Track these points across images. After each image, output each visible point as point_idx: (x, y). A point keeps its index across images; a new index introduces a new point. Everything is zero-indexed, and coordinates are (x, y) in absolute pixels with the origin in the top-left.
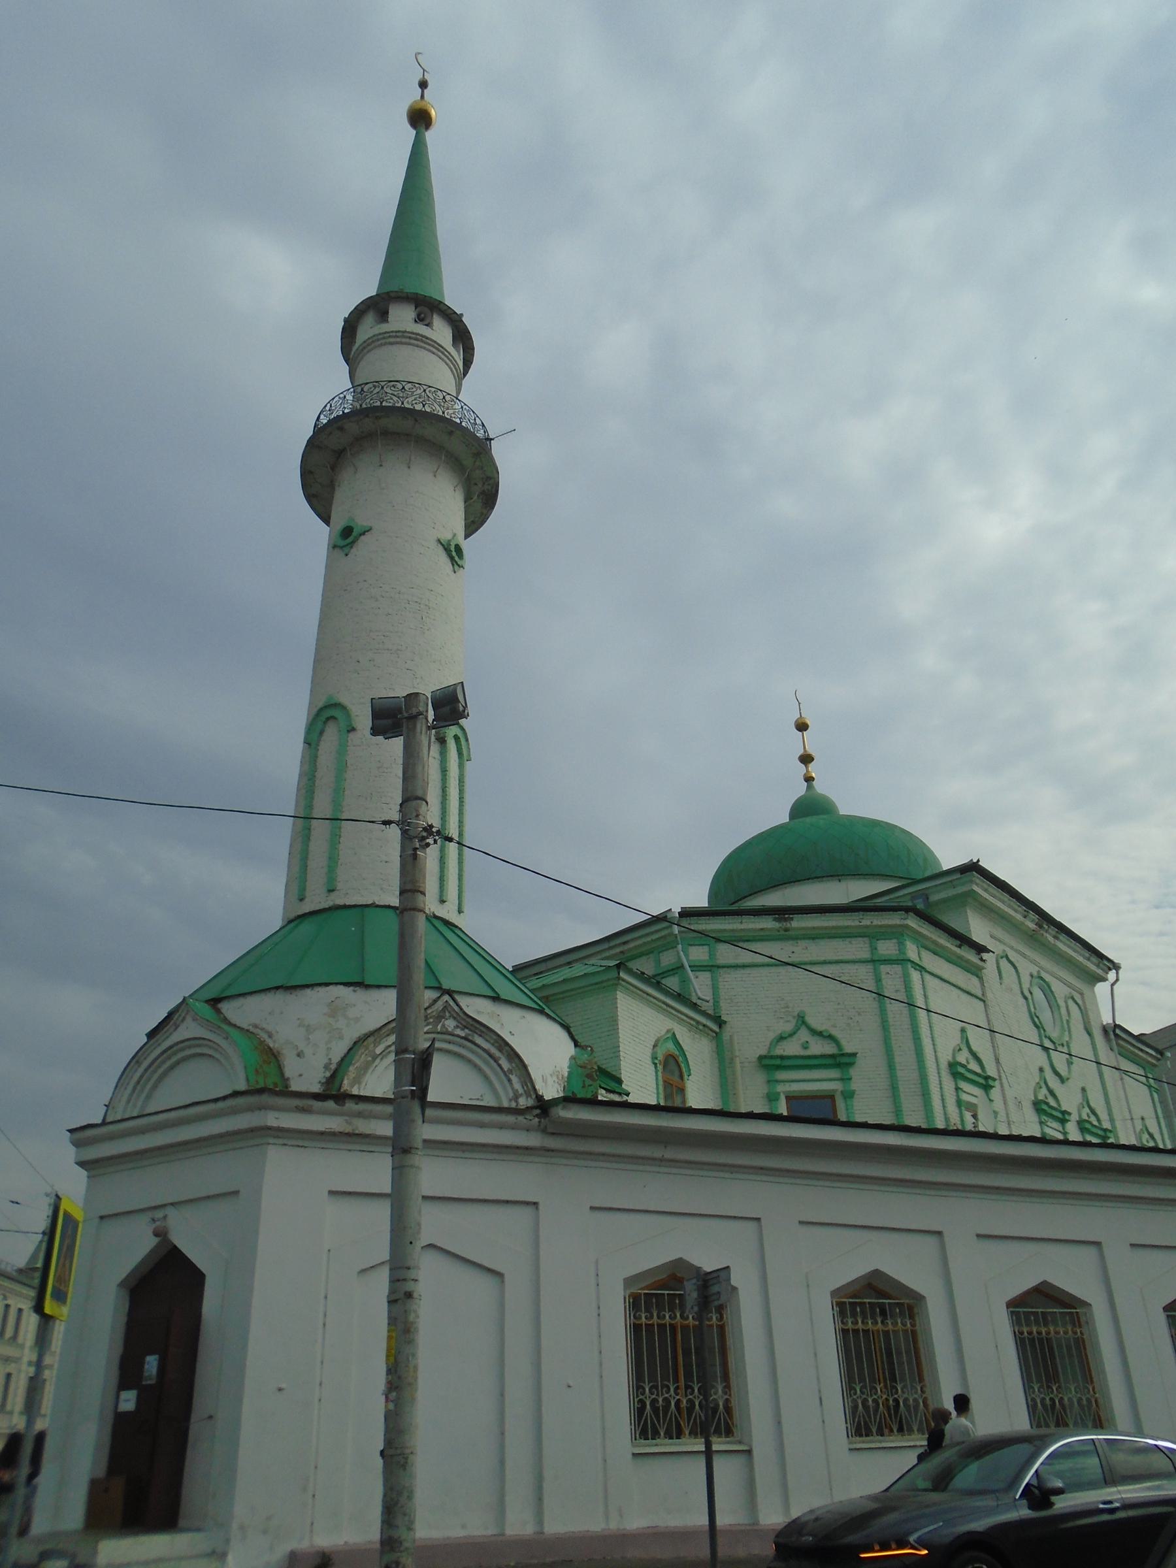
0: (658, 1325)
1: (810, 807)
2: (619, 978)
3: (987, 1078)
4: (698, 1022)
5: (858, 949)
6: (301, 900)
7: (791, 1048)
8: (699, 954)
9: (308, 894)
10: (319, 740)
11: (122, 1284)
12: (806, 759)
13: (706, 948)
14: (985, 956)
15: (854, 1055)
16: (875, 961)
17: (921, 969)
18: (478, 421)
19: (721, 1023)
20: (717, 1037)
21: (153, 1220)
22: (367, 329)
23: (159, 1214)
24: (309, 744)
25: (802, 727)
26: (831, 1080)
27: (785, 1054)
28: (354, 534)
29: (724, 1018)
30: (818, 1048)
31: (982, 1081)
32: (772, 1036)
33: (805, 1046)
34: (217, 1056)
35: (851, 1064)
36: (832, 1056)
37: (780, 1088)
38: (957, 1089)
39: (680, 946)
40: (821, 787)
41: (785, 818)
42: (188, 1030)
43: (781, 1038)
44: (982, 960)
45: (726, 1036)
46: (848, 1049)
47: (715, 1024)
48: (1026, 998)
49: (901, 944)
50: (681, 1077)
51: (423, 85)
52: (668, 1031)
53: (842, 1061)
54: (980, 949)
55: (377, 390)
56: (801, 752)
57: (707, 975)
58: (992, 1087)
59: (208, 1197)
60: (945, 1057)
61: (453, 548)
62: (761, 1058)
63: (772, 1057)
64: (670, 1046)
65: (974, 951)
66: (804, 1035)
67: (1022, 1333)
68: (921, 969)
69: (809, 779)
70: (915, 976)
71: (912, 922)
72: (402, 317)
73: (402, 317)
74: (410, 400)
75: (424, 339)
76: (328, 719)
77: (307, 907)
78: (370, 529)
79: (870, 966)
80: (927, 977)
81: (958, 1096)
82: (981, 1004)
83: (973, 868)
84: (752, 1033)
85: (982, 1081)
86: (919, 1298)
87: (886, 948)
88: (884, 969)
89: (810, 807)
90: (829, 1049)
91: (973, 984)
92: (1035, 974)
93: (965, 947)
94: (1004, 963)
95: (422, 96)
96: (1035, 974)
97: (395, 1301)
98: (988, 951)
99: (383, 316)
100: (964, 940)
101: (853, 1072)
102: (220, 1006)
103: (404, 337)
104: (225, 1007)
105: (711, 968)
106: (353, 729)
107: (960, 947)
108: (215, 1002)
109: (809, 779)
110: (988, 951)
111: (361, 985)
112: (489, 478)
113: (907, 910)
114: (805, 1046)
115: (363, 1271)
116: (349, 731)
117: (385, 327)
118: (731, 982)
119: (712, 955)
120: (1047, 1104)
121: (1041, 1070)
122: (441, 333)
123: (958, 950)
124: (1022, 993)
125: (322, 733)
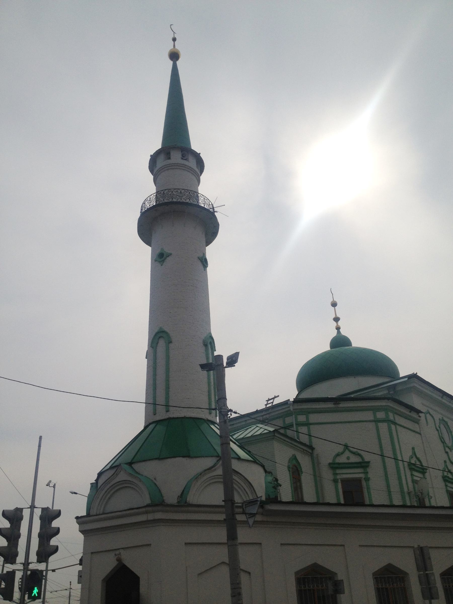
0: (308, 590)
1: (340, 342)
2: (274, 436)
3: (423, 469)
4: (304, 450)
5: (369, 415)
6: (155, 415)
7: (342, 459)
8: (301, 418)
9: (157, 412)
10: (157, 346)
11: (103, 580)
12: (337, 319)
13: (305, 416)
14: (420, 414)
15: (369, 462)
16: (377, 421)
17: (395, 424)
18: (210, 203)
19: (312, 448)
20: (311, 455)
21: (116, 555)
22: (160, 163)
23: (117, 552)
24: (153, 348)
25: (334, 305)
26: (359, 473)
27: (340, 462)
28: (165, 256)
29: (314, 446)
30: (354, 459)
31: (421, 470)
32: (334, 454)
33: (348, 458)
34: (136, 488)
35: (368, 466)
36: (360, 463)
37: (338, 477)
38: (412, 475)
39: (294, 416)
40: (344, 332)
41: (327, 348)
42: (122, 476)
43: (338, 455)
44: (420, 417)
45: (315, 455)
46: (367, 459)
47: (309, 449)
48: (437, 430)
49: (387, 414)
50: (299, 475)
51: (174, 40)
52: (293, 455)
53: (364, 465)
54: (418, 412)
55: (170, 193)
56: (334, 316)
57: (306, 427)
58: (425, 472)
59: (137, 546)
60: (406, 459)
61: (204, 260)
62: (330, 464)
63: (334, 464)
64: (294, 462)
65: (416, 413)
66: (347, 453)
67: (446, 586)
68: (395, 424)
69: (338, 328)
70: (393, 427)
71: (391, 404)
72: (176, 157)
73: (176, 157)
74: (184, 197)
75: (185, 166)
76: (160, 337)
77: (158, 418)
78: (171, 254)
79: (374, 423)
80: (398, 427)
81: (412, 478)
82: (419, 435)
83: (414, 377)
84: (326, 452)
85: (421, 470)
86: (406, 574)
87: (381, 415)
88: (380, 424)
89: (340, 342)
90: (358, 460)
91: (416, 427)
92: (441, 418)
93: (412, 412)
94: (428, 415)
95: (174, 46)
96: (441, 418)
97: (234, 596)
98: (422, 412)
99: (168, 157)
100: (412, 409)
101: (368, 470)
102: (133, 465)
103: (177, 166)
104: (135, 466)
105: (307, 424)
106: (171, 342)
107: (410, 412)
108: (130, 464)
109: (338, 328)
110: (422, 412)
111: (189, 457)
112: (215, 227)
113: (388, 399)
114: (348, 458)
115: (199, 574)
116: (169, 343)
117: (169, 162)
118: (315, 430)
119: (307, 418)
120: (448, 477)
121: (445, 462)
122: (192, 163)
123: (409, 414)
124: (436, 428)
125: (157, 343)
